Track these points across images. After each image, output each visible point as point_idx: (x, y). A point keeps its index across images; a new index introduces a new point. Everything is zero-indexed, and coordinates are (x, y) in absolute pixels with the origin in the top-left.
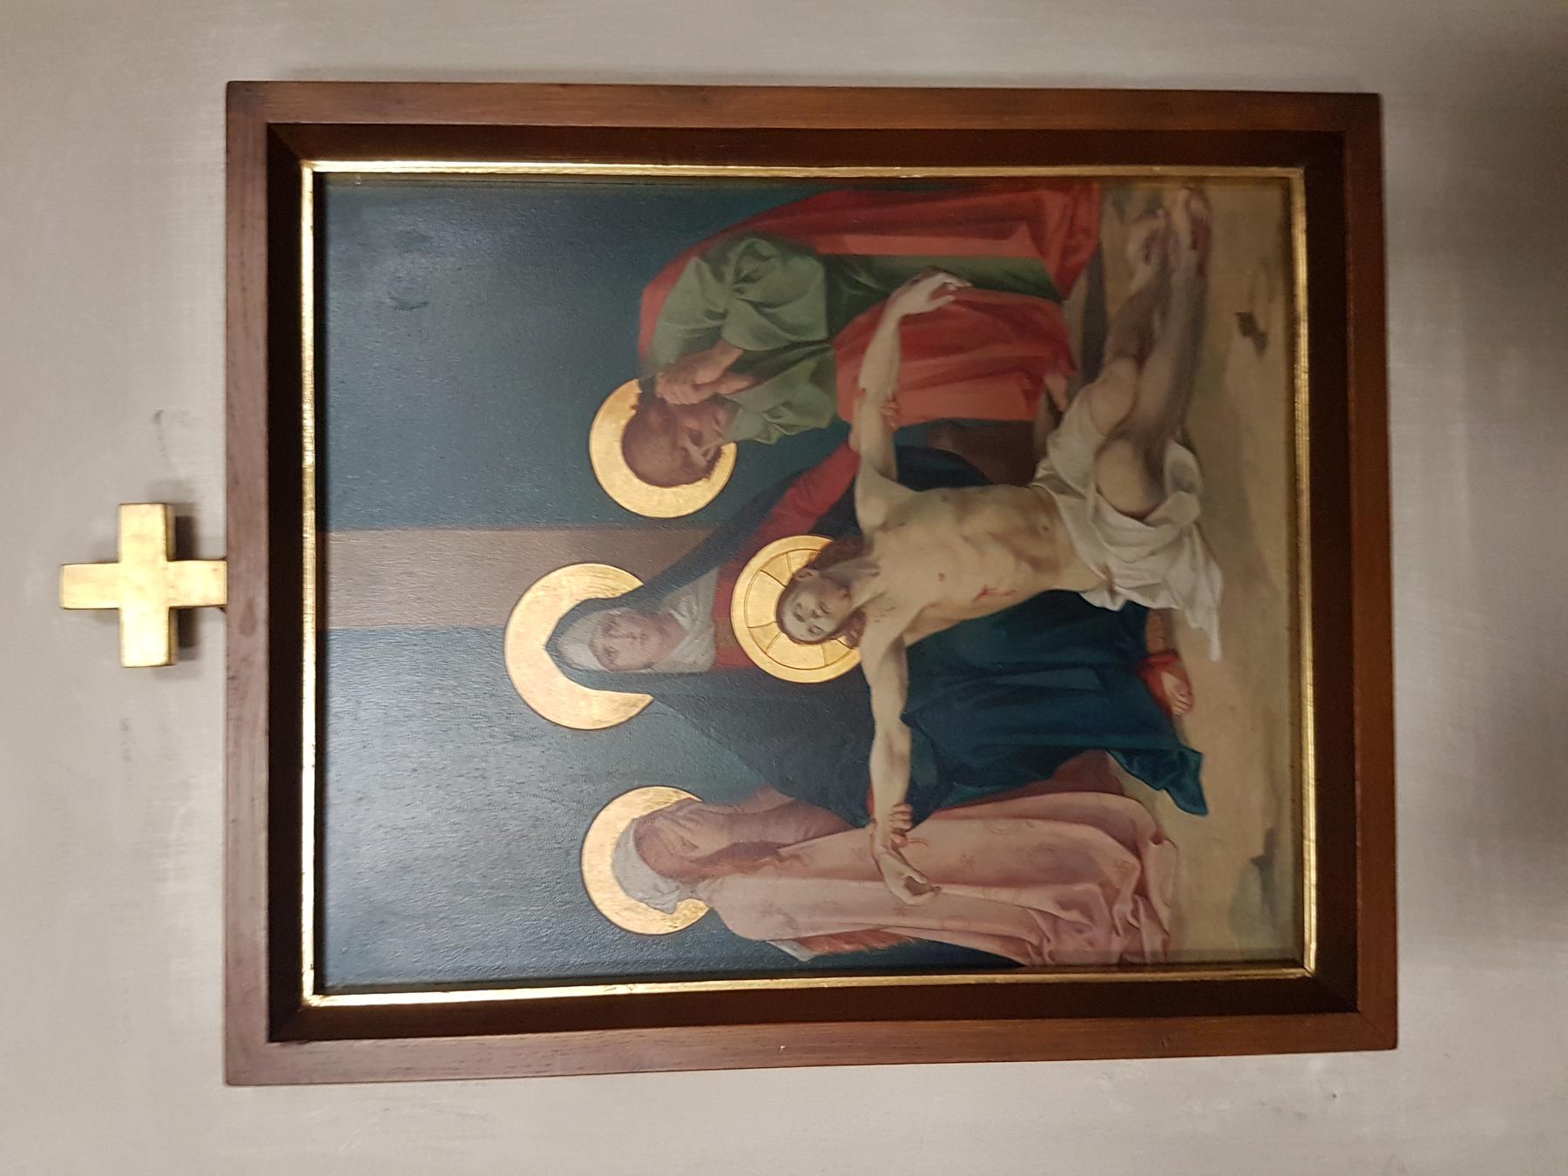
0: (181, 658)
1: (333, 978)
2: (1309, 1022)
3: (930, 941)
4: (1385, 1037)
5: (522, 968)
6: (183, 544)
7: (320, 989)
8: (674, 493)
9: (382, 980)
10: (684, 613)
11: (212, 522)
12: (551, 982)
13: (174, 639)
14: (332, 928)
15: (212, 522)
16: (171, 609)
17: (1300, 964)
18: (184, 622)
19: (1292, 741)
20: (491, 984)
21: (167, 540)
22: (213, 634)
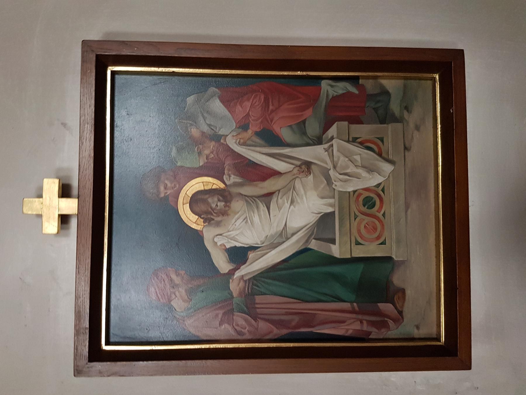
0: (65, 226)
1: (112, 340)
7: (108, 343)
18: (64, 219)
19: (434, 176)
22: (74, 223)
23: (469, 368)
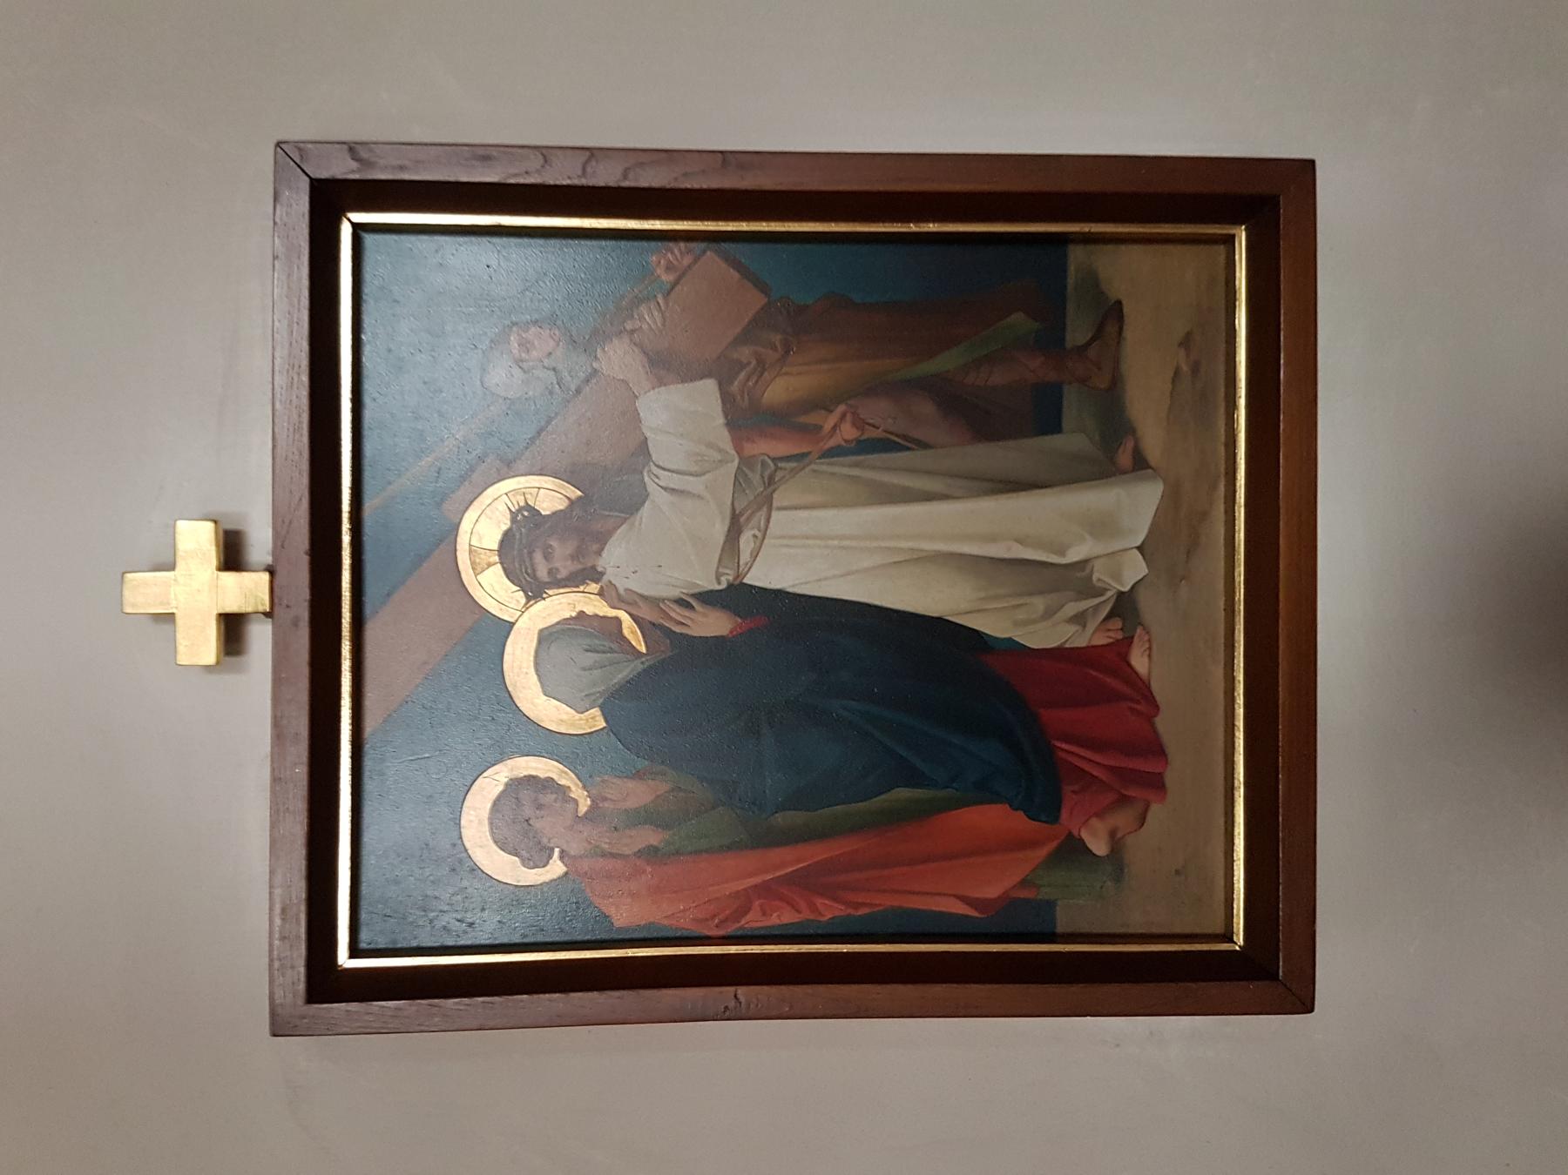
1: (365, 940)
2: (1113, 989)
3: (962, 915)
4: (1303, 1002)
5: (649, 925)
6: (232, 556)
8: (556, 707)
9: (450, 942)
10: (445, 909)
11: (260, 544)
12: (726, 941)
13: (222, 648)
14: (364, 884)
15: (260, 544)
16: (220, 615)
17: (1228, 937)
18: (232, 628)
20: (588, 945)
21: (219, 559)
22: (260, 637)
23: (1308, 166)
